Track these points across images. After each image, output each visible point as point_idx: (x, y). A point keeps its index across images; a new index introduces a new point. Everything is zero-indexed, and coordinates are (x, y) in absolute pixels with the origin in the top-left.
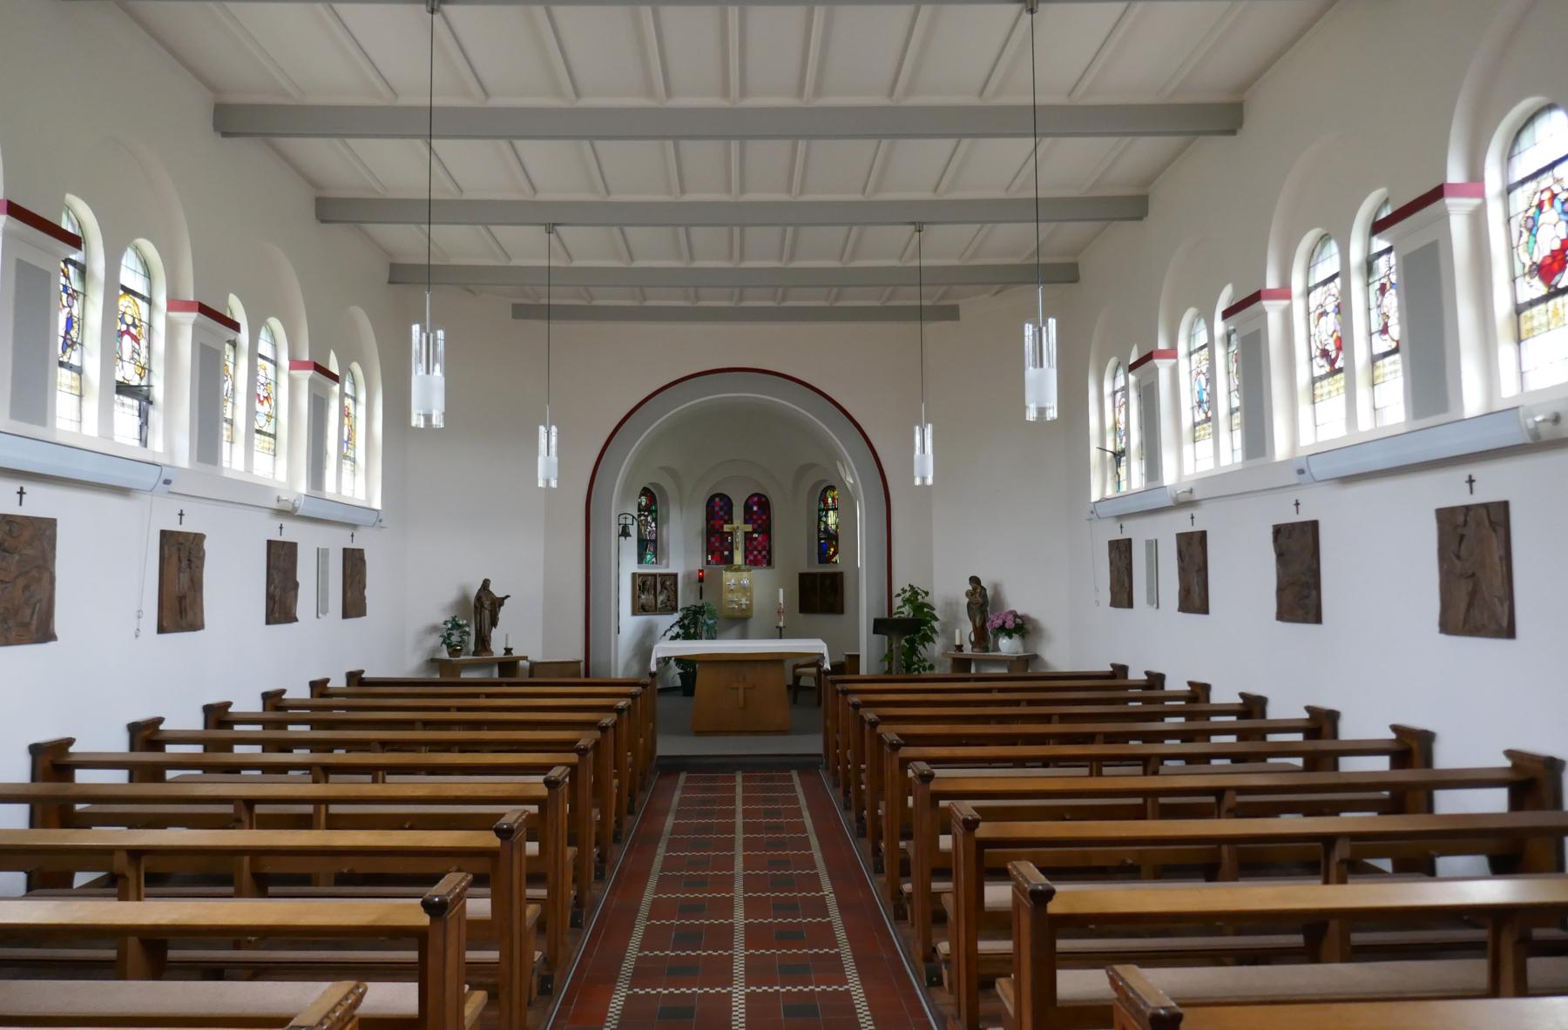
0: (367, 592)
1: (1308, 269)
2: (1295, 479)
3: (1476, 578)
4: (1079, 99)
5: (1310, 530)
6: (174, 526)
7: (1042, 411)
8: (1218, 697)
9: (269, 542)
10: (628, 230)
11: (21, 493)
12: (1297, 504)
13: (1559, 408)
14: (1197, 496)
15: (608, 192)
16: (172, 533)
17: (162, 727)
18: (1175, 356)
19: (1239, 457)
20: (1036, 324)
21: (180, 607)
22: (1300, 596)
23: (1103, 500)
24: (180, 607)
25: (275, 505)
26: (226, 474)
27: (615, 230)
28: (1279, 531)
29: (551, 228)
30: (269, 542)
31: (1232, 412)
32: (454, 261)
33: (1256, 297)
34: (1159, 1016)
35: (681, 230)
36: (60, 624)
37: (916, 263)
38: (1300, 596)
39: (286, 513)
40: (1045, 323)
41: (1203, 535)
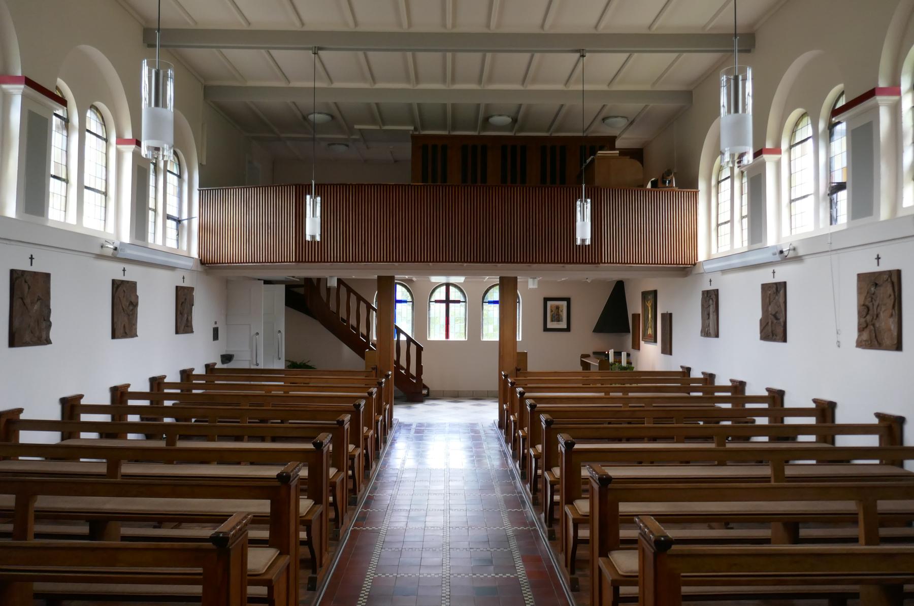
0: (759, 315)
1: (793, 132)
2: (778, 258)
3: (877, 321)
4: (654, 30)
5: (894, 279)
6: (24, 266)
7: (583, 241)
8: (719, 382)
9: (177, 287)
10: (370, 54)
11: (124, 270)
12: (878, 258)
13: (794, 245)
14: (801, 252)
15: (374, 80)
16: (23, 272)
17: (194, 373)
18: (898, 93)
19: (746, 244)
20: (581, 201)
21: (124, 322)
22: (774, 327)
23: (709, 260)
24: (124, 322)
25: (98, 251)
26: (49, 224)
27: (361, 54)
28: (765, 287)
29: (316, 50)
30: (177, 287)
31: (742, 218)
32: (250, 83)
33: (871, 94)
34: (661, 541)
35: (409, 54)
36: (139, 331)
37: (580, 87)
38: (774, 327)
39: (117, 255)
40: (586, 201)
41: (716, 292)
